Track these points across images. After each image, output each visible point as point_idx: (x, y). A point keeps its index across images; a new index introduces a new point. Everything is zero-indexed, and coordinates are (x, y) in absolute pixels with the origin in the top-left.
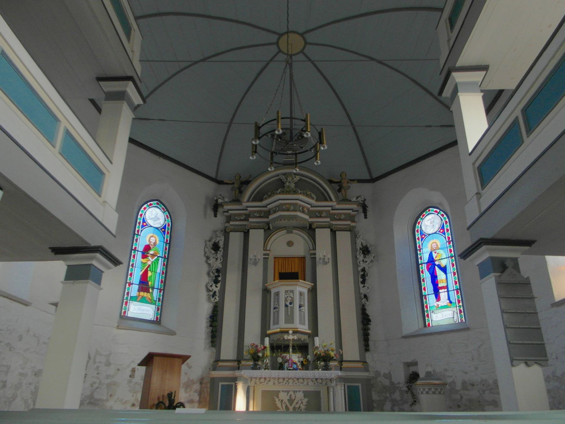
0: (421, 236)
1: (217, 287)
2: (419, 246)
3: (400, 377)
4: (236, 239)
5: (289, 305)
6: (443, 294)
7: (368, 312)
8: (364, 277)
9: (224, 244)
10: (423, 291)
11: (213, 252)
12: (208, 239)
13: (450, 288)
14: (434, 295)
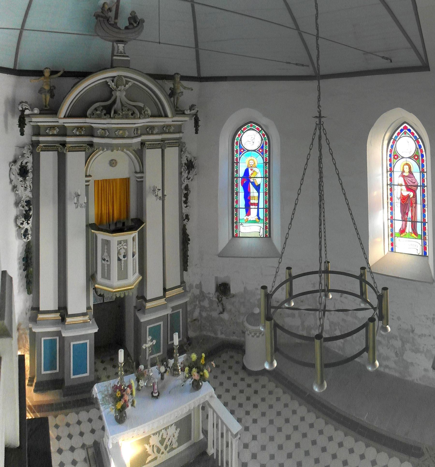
0: (240, 150)
1: (28, 224)
2: (237, 159)
3: (210, 288)
4: (48, 160)
5: (123, 259)
6: (254, 212)
7: (188, 232)
8: (186, 196)
9: (33, 167)
10: (235, 204)
11: (21, 179)
12: (11, 159)
13: (261, 206)
14: (244, 210)
